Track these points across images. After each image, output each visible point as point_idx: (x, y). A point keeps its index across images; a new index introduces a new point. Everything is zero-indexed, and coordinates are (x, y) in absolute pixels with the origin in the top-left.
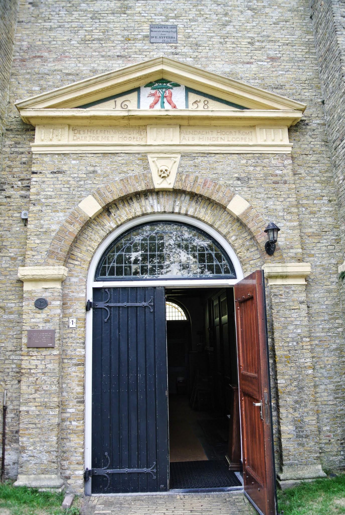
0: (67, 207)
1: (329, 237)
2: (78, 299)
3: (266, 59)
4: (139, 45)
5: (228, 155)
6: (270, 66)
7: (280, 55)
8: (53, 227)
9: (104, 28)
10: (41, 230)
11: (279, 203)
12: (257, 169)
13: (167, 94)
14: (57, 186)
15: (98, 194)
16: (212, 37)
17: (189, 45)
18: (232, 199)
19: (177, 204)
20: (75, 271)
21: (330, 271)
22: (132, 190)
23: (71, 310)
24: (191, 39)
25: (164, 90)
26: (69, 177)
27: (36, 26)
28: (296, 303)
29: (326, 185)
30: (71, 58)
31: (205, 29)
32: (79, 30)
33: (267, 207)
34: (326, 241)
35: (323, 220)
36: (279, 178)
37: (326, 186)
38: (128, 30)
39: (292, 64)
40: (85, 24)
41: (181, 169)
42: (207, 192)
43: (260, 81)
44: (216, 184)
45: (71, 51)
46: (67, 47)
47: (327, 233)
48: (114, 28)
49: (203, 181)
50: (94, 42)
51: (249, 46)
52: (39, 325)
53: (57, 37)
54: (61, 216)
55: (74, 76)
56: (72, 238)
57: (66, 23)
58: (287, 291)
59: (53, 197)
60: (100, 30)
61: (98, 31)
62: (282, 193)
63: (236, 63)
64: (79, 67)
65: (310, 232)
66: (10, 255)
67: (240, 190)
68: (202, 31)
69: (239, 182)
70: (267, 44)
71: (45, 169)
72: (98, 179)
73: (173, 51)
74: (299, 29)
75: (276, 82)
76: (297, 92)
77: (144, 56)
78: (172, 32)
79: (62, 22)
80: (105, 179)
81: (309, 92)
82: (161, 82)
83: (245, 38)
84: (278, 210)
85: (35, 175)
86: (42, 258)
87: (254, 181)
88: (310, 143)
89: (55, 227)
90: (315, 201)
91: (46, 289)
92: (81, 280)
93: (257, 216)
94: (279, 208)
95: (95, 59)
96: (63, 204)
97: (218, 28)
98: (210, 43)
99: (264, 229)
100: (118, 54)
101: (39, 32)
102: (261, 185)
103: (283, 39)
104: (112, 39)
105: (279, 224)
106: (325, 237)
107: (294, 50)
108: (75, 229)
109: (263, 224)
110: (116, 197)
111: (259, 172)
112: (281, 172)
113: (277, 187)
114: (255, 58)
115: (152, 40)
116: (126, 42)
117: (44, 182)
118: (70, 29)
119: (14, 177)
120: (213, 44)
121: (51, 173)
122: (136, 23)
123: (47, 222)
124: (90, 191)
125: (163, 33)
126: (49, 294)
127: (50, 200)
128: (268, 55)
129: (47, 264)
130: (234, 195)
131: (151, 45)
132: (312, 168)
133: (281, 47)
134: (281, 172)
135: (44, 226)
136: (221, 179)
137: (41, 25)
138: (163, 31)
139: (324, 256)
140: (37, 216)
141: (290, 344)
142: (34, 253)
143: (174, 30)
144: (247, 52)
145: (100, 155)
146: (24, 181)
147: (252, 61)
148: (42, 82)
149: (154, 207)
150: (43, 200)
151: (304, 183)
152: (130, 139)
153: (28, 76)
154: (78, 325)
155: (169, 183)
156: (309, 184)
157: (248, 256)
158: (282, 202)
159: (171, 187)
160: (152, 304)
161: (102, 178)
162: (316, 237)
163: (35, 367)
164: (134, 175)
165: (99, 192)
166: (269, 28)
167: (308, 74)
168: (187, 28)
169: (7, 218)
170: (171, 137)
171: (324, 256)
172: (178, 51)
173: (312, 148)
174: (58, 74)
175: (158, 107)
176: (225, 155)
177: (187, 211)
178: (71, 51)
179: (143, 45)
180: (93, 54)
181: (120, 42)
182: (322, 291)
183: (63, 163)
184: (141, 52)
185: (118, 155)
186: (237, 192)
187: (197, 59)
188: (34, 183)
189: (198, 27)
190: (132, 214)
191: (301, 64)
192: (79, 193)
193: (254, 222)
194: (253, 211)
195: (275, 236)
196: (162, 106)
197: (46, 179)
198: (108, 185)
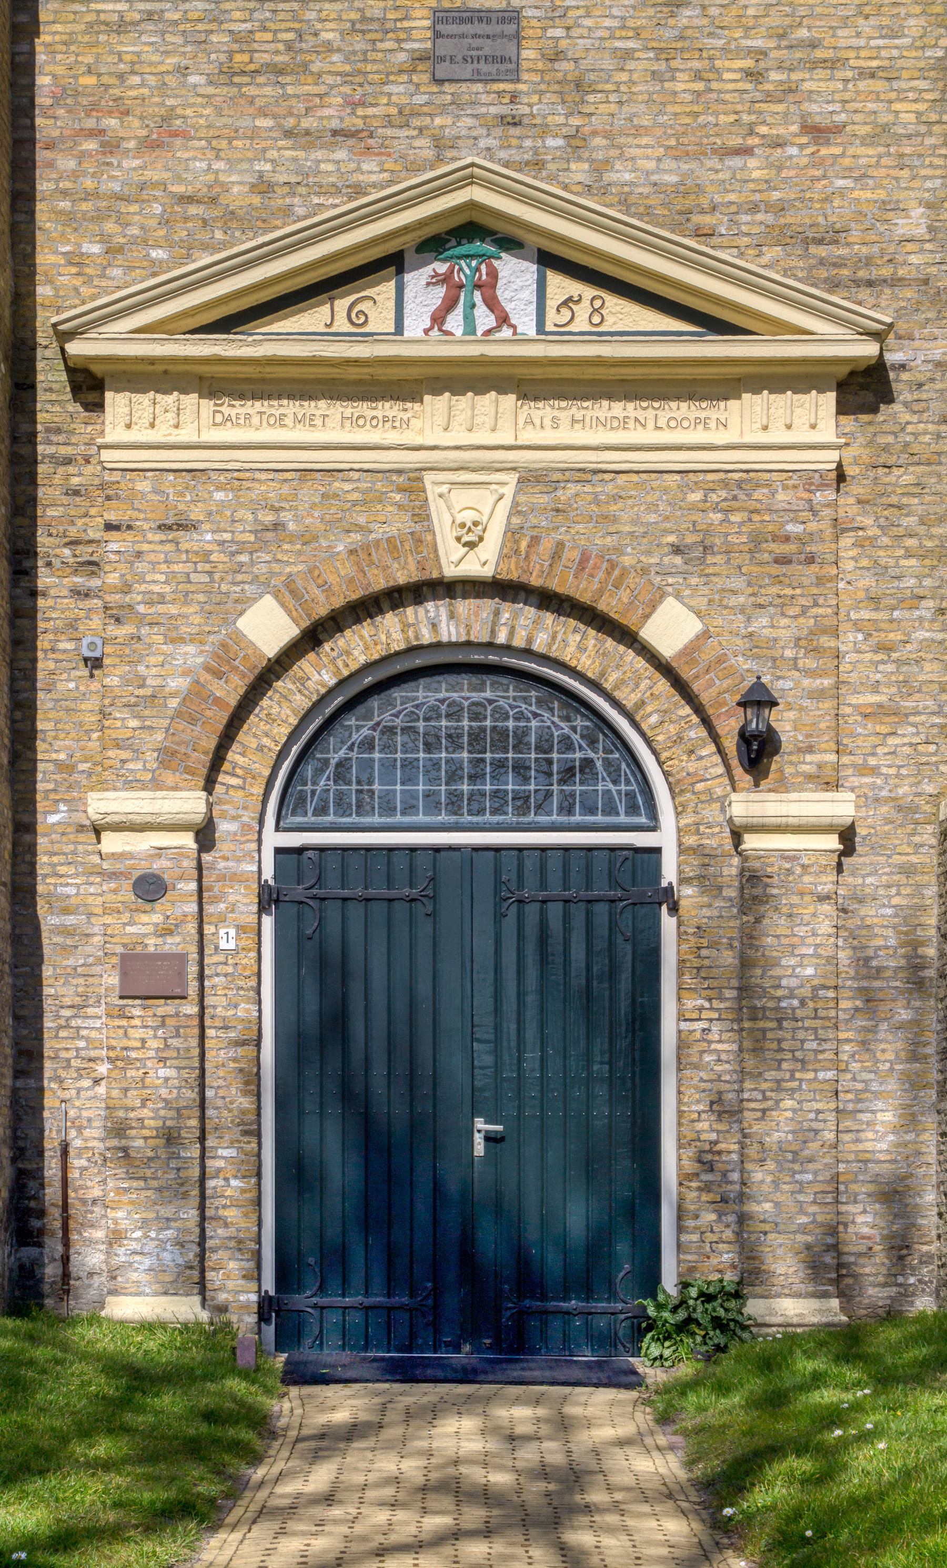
0: (207, 629)
1: (923, 718)
2: (236, 878)
3: (796, 135)
5: (654, 476)
6: (805, 160)
7: (843, 117)
10: (141, 692)
14: (175, 568)
15: (289, 593)
16: (628, 54)
19: (503, 621)
20: (228, 802)
22: (379, 583)
23: (222, 906)
25: (474, 263)
27: (75, 13)
28: (807, 898)
29: (935, 563)
31: (607, 23)
33: (751, 634)
37: (934, 567)
38: (363, 32)
41: (516, 520)
42: (586, 590)
43: (769, 218)
44: (613, 565)
45: (189, 112)
46: (176, 96)
48: (319, 26)
49: (576, 555)
50: (261, 79)
51: (749, 86)
52: (147, 941)
54: (192, 655)
55: (202, 207)
58: (788, 866)
59: (168, 598)
60: (275, 32)
63: (699, 155)
65: (871, 705)
66: (54, 756)
68: (599, 33)
69: (678, 560)
70: (807, 76)
72: (286, 547)
75: (821, 220)
78: (503, 36)
81: (922, 251)
82: (467, 233)
84: (782, 644)
86: (145, 769)
88: (903, 429)
89: (179, 684)
90: (896, 614)
92: (245, 827)
93: (721, 660)
95: (264, 144)
96: (197, 619)
98: (624, 77)
99: (738, 697)
100: (335, 124)
101: (86, 38)
102: (740, 567)
103: (863, 54)
107: (893, 95)
108: (230, 691)
110: (338, 602)
112: (802, 527)
114: (763, 130)
115: (443, 70)
117: (139, 554)
118: (182, 27)
119: (50, 535)
120: (632, 82)
121: (159, 527)
123: (154, 671)
124: (267, 584)
126: (168, 864)
127: (161, 608)
129: (156, 784)
131: (435, 89)
132: (899, 508)
133: (850, 86)
134: (799, 528)
136: (629, 550)
137: (89, 11)
138: (475, 36)
139: (904, 771)
140: (127, 651)
141: (783, 1004)
142: (124, 755)
143: (510, 29)
146: (80, 547)
148: (110, 227)
149: (437, 623)
150: (141, 609)
151: (870, 557)
152: (374, 422)
153: (65, 205)
154: (243, 943)
157: (691, 770)
159: (487, 572)
160: (430, 892)
162: (887, 719)
163: (139, 1045)
165: (293, 586)
167: (929, 184)
170: (492, 420)
173: (907, 444)
174: (156, 199)
176: (644, 476)
177: (530, 640)
178: (189, 112)
180: (258, 123)
182: (887, 870)
186: (670, 589)
187: (579, 143)
188: (113, 557)
191: (908, 150)
192: (238, 589)
198: (316, 567)
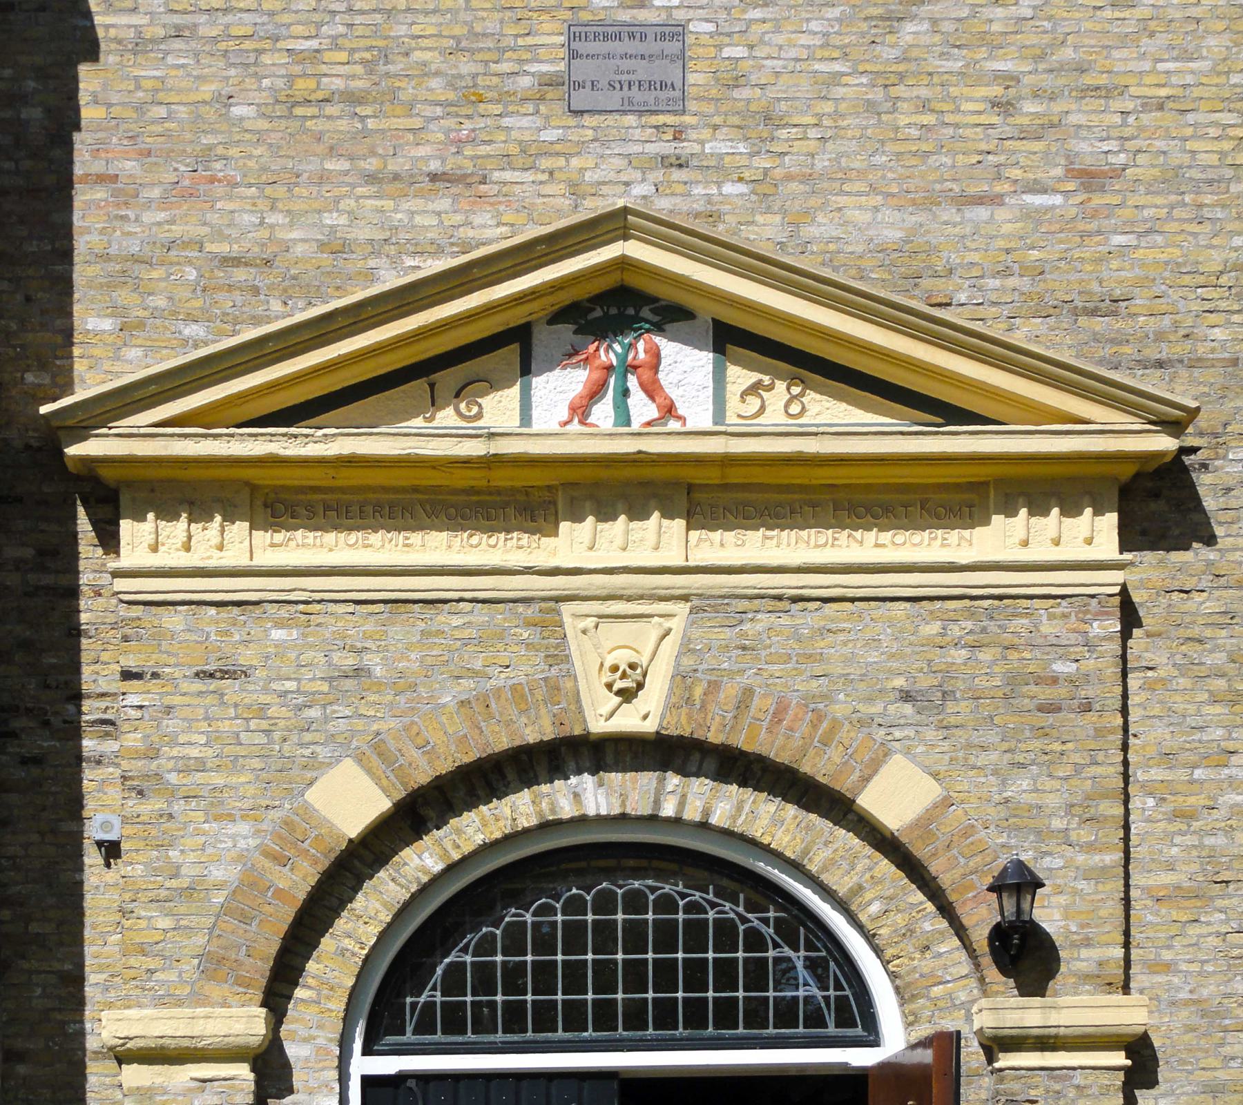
0: (264, 803)
3: (1059, 180)
4: (522, 124)
6: (1074, 211)
8: (215, 873)
9: (369, 42)
10: (174, 883)
11: (1056, 784)
12: (981, 656)
13: (642, 355)
15: (377, 755)
17: (736, 120)
18: (876, 771)
19: (670, 788)
21: (1227, 1022)
22: (501, 741)
24: (745, 93)
26: (266, 690)
30: (236, 185)
31: (804, 40)
32: (264, 51)
33: (1007, 801)
34: (1223, 917)
35: (1220, 840)
36: (1062, 691)
38: (472, 52)
39: (1173, 198)
40: (286, 18)
41: (688, 662)
42: (783, 748)
43: (1024, 283)
44: (819, 717)
46: (214, 132)
47: (1232, 886)
50: (329, 110)
51: (995, 120)
53: (170, 83)
54: (243, 837)
56: (287, 914)
57: (203, 18)
58: (1057, 1087)
59: (209, 765)
60: (352, 51)
61: (343, 56)
62: (1070, 746)
63: (930, 201)
64: (272, 226)
65: (1165, 887)
67: (908, 738)
68: (793, 53)
69: (908, 709)
70: (1074, 107)
71: (172, 661)
72: (372, 698)
73: (667, 148)
74: (1221, 26)
75: (1094, 286)
76: (1176, 325)
77: (545, 177)
78: (663, 56)
79: (185, 12)
80: (402, 699)
83: (979, 81)
84: (1048, 811)
85: (135, 682)
87: (963, 704)
90: (1198, 773)
91: (204, 1081)
93: (968, 832)
94: (1052, 801)
97: (863, 34)
98: (828, 107)
99: (989, 880)
100: (434, 166)
102: (991, 718)
104: (402, 96)
105: (1048, 859)
106: (1219, 903)
107: (1189, 131)
109: (988, 859)
111: (988, 670)
112: (1074, 665)
113: (1052, 727)
114: (1016, 173)
115: (581, 99)
116: (464, 111)
117: (169, 709)
119: (48, 687)
121: (197, 674)
122: (508, 14)
123: (192, 857)
125: (627, 69)
127: (199, 777)
128: (1070, 157)
129: (198, 999)
130: (886, 755)
131: (572, 121)
132: (1200, 641)
133: (1131, 119)
135: (184, 871)
136: (841, 696)
138: (625, 56)
140: (154, 833)
143: (673, 47)
144: (984, 146)
145: (381, 607)
147: (998, 188)
155: (643, 712)
156: (1179, 707)
157: (926, 970)
158: (1066, 779)
159: (649, 727)
161: (390, 698)
162: (1187, 903)
164: (510, 682)
166: (1088, 25)
168: (729, 35)
169: (35, 837)
171: (1211, 969)
172: (688, 148)
174: (190, 262)
175: (603, 413)
177: (707, 812)
178: (233, 152)
179: (539, 122)
181: (439, 111)
182: (1188, 1089)
183: (237, 637)
184: (528, 155)
185: (447, 606)
189: (777, 30)
190: (501, 823)
191: (1208, 199)
192: (307, 752)
193: (955, 851)
194: (955, 812)
195: (1026, 905)
196: (623, 416)
197: (177, 700)
198: (413, 723)
